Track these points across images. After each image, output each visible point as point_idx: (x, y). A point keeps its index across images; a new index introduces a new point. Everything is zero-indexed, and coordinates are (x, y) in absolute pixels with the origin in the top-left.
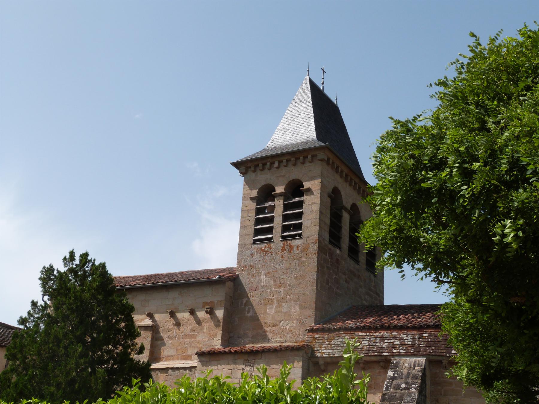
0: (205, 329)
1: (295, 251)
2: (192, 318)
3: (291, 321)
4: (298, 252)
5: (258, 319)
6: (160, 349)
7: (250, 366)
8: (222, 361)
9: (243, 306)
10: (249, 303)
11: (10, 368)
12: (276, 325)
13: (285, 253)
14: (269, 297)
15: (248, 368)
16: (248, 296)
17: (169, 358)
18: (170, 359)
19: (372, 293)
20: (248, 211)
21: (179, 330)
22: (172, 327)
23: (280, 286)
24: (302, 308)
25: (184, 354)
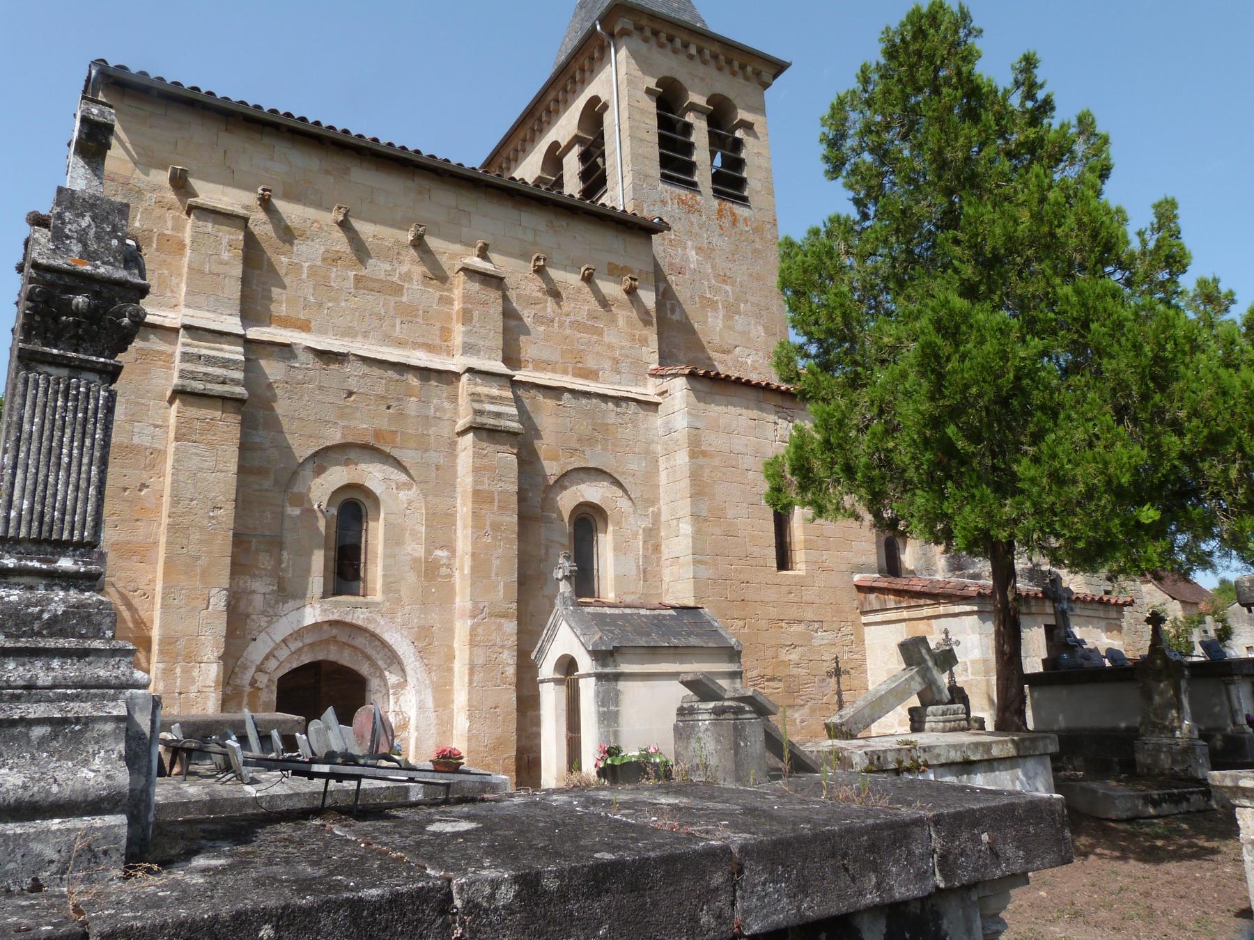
0: (621, 322)
1: (741, 225)
2: (586, 289)
3: (754, 352)
5: (693, 332)
6: (517, 340)
7: (786, 419)
11: (450, 290)
12: (728, 352)
16: (666, 281)
17: (544, 365)
21: (560, 307)
22: (540, 295)
25: (579, 365)
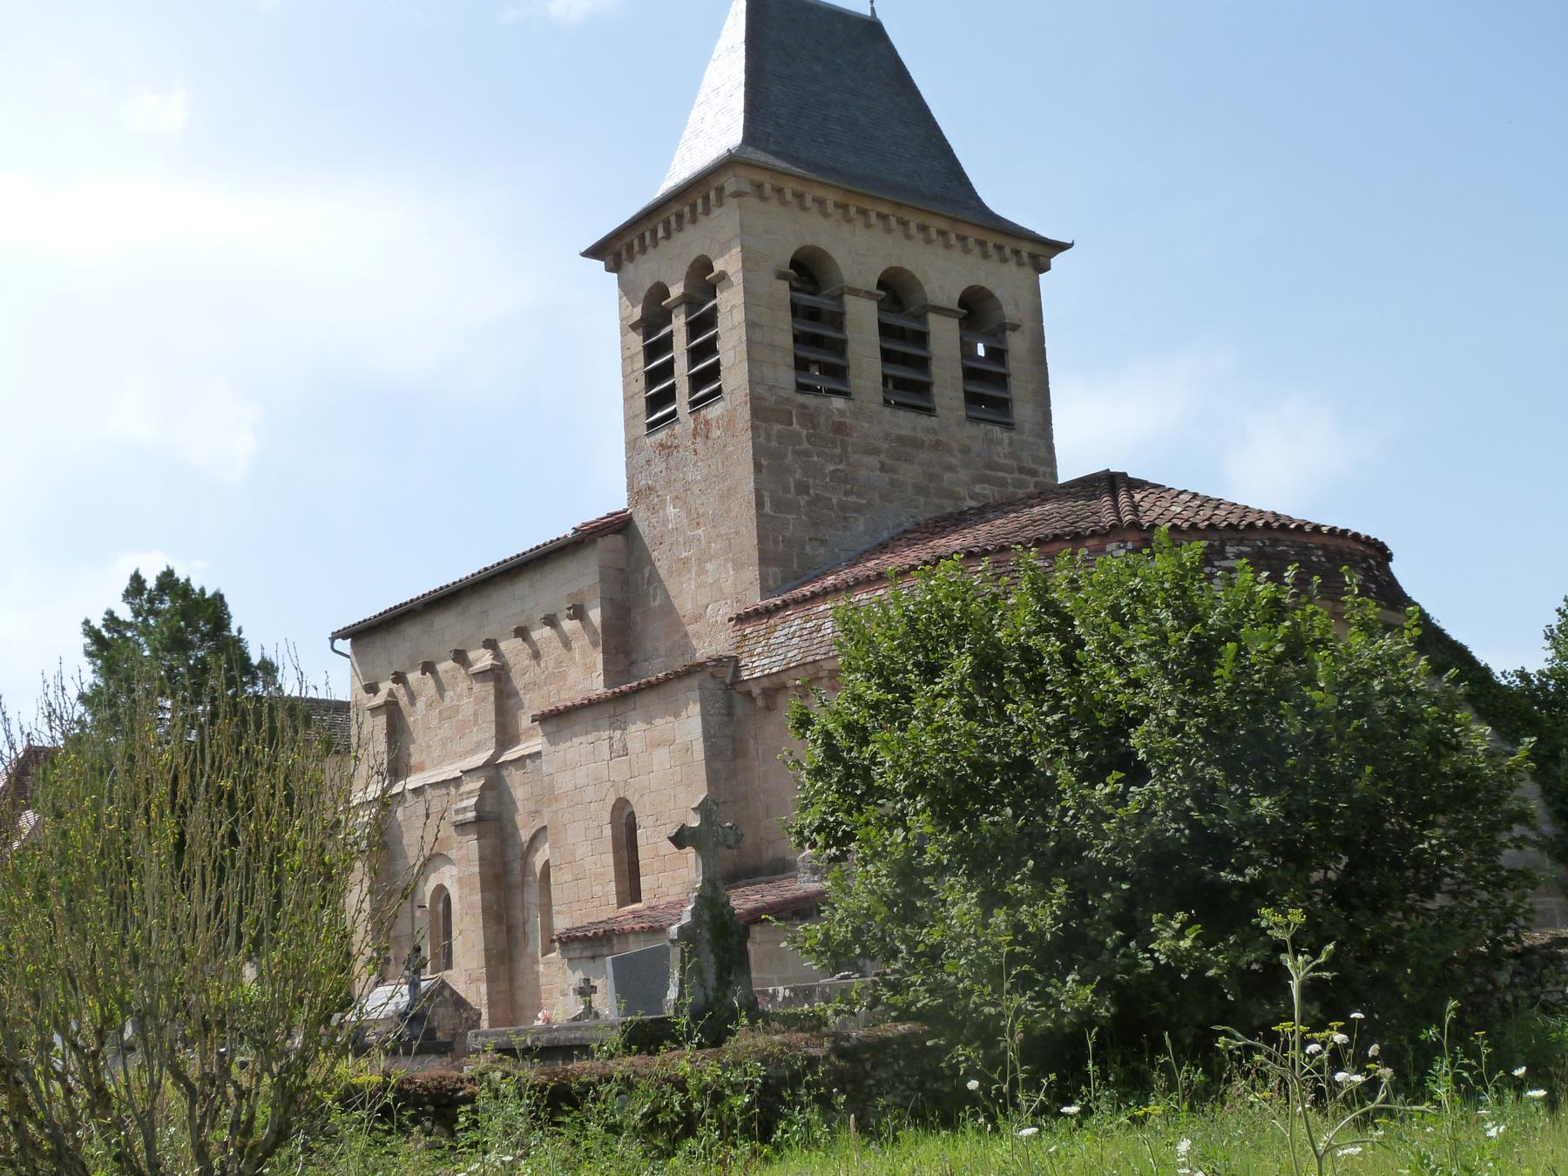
1: (715, 433)
4: (719, 433)
8: (576, 728)
9: (645, 587)
10: (654, 577)
13: (700, 446)
14: (685, 554)
15: (618, 734)
18: (532, 736)
19: (1001, 474)
20: (632, 357)
23: (698, 524)
24: (738, 567)
